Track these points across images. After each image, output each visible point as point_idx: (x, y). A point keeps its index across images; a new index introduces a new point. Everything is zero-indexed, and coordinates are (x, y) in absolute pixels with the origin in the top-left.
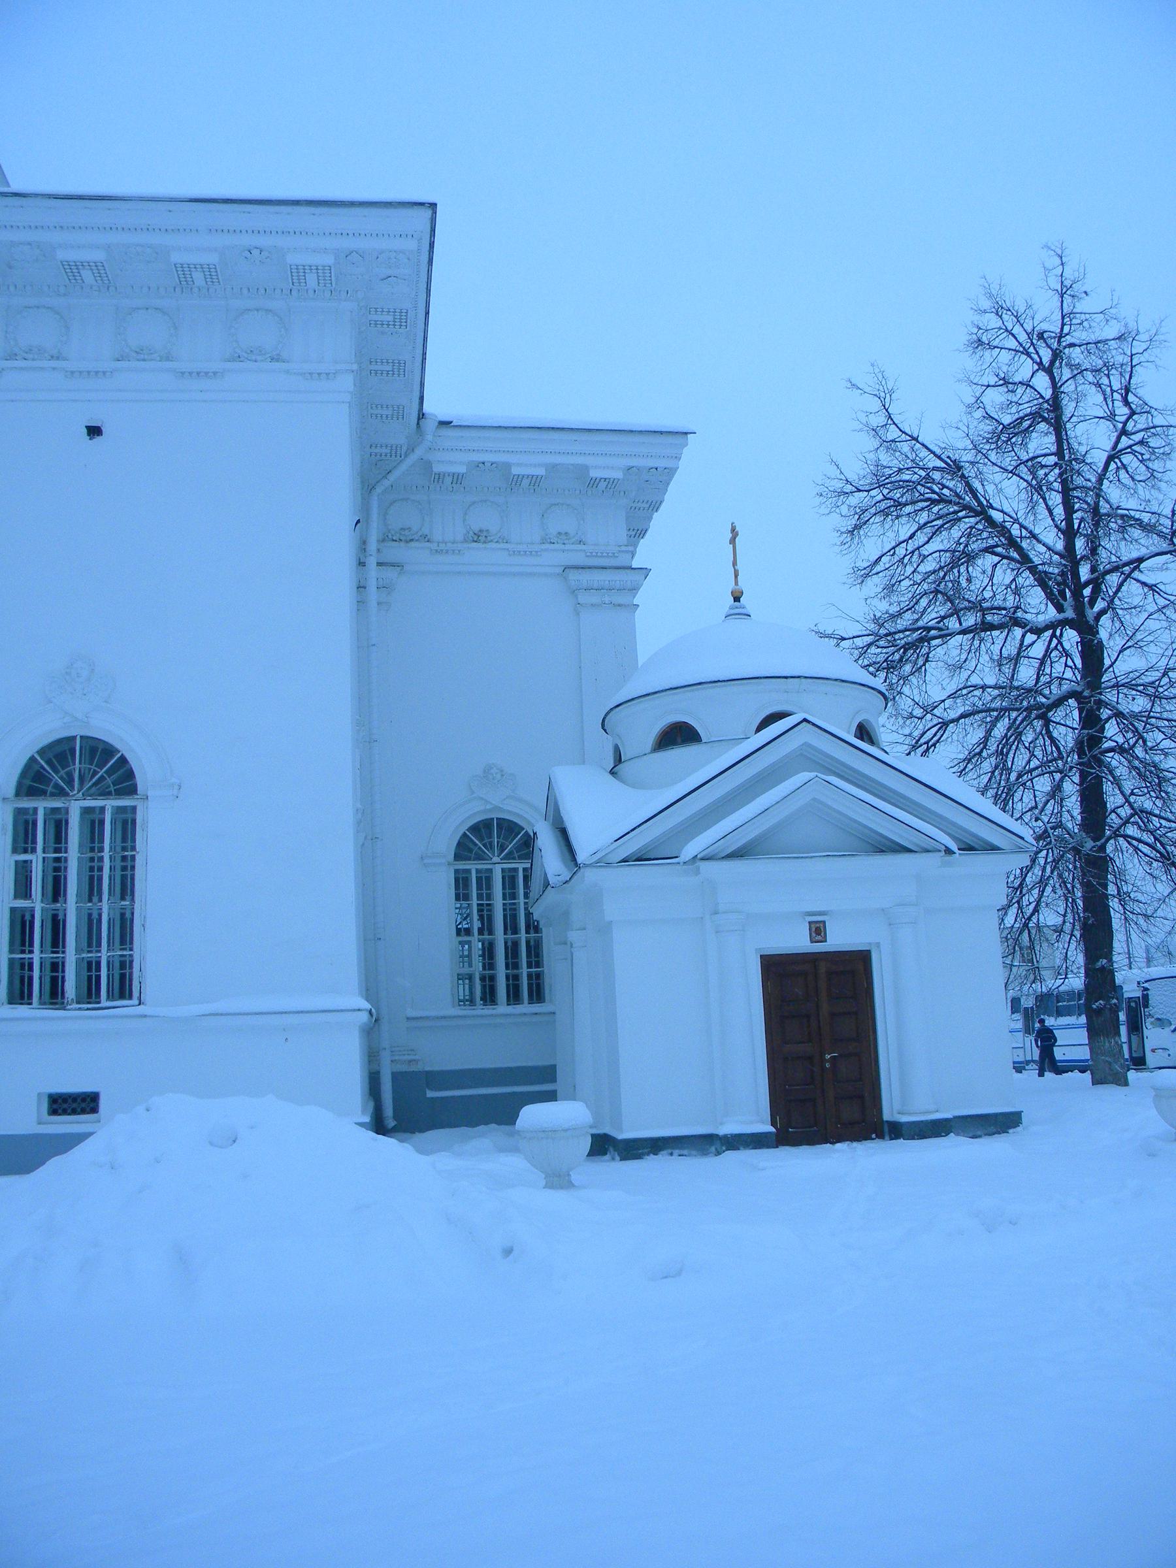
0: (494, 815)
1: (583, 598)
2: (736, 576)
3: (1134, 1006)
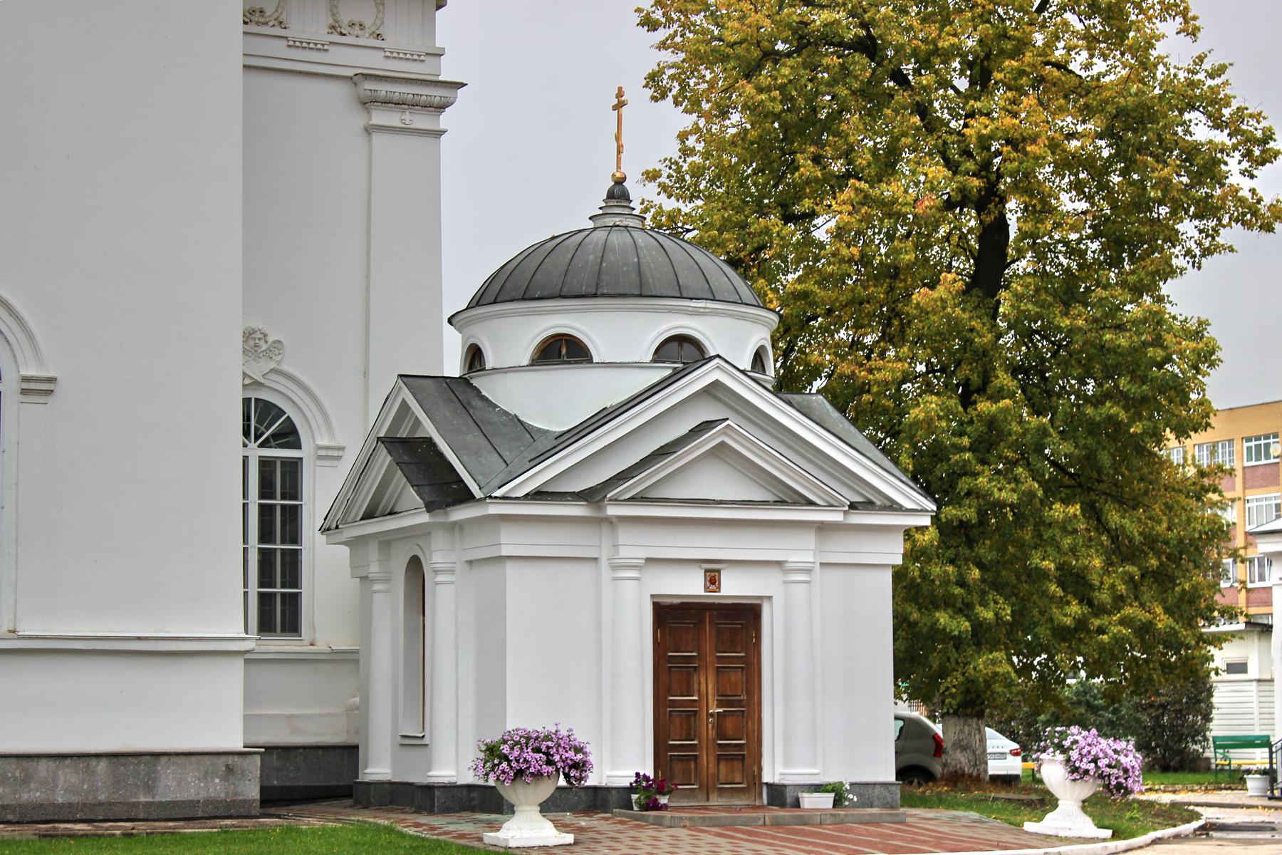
0: (290, 411)
1: (380, 117)
2: (619, 152)
3: (1040, 43)
